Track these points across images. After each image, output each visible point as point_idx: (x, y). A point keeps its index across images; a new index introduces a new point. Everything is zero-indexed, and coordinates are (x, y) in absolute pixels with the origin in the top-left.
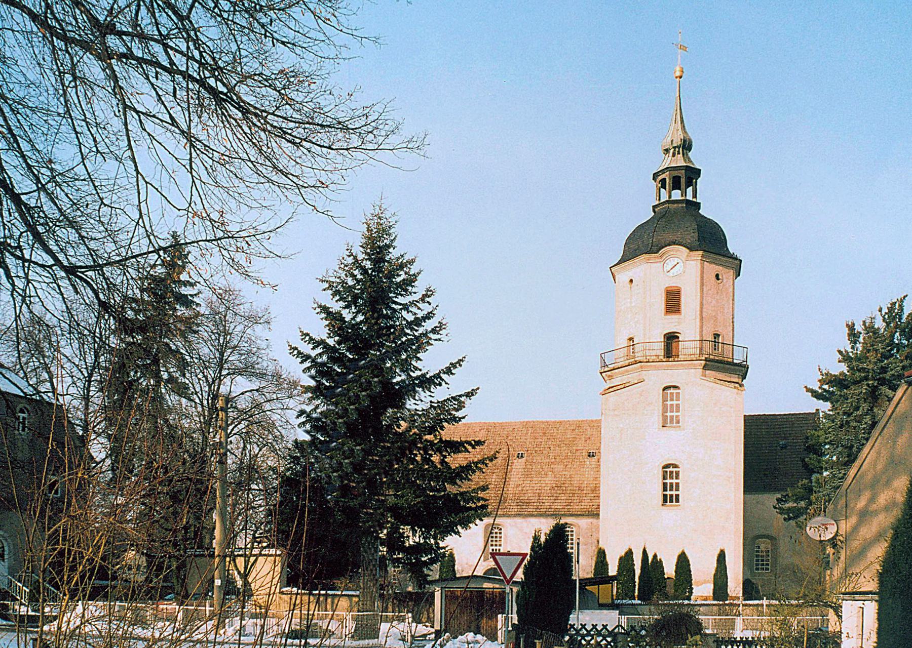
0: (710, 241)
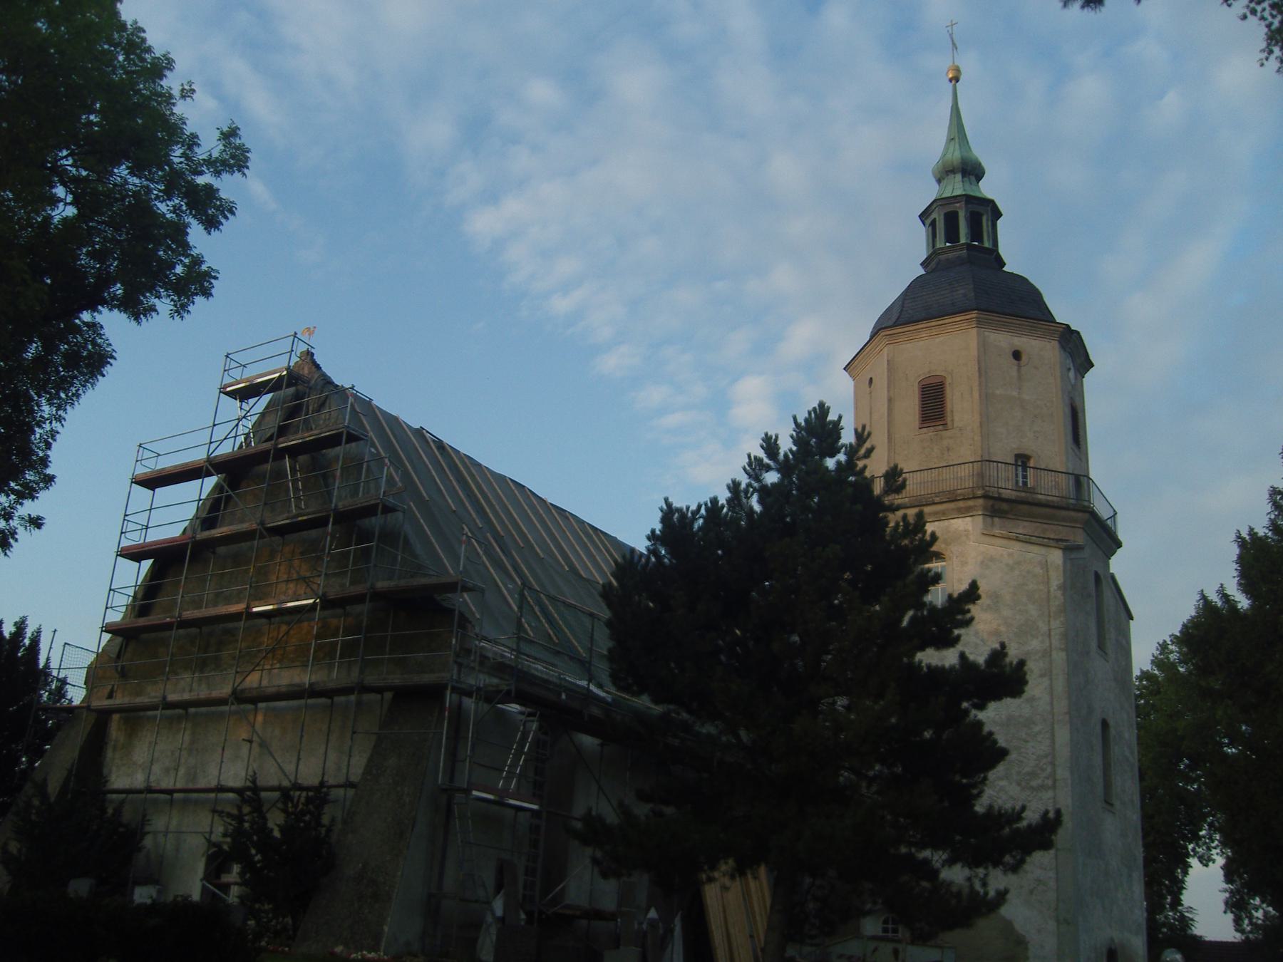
0: (1018, 304)
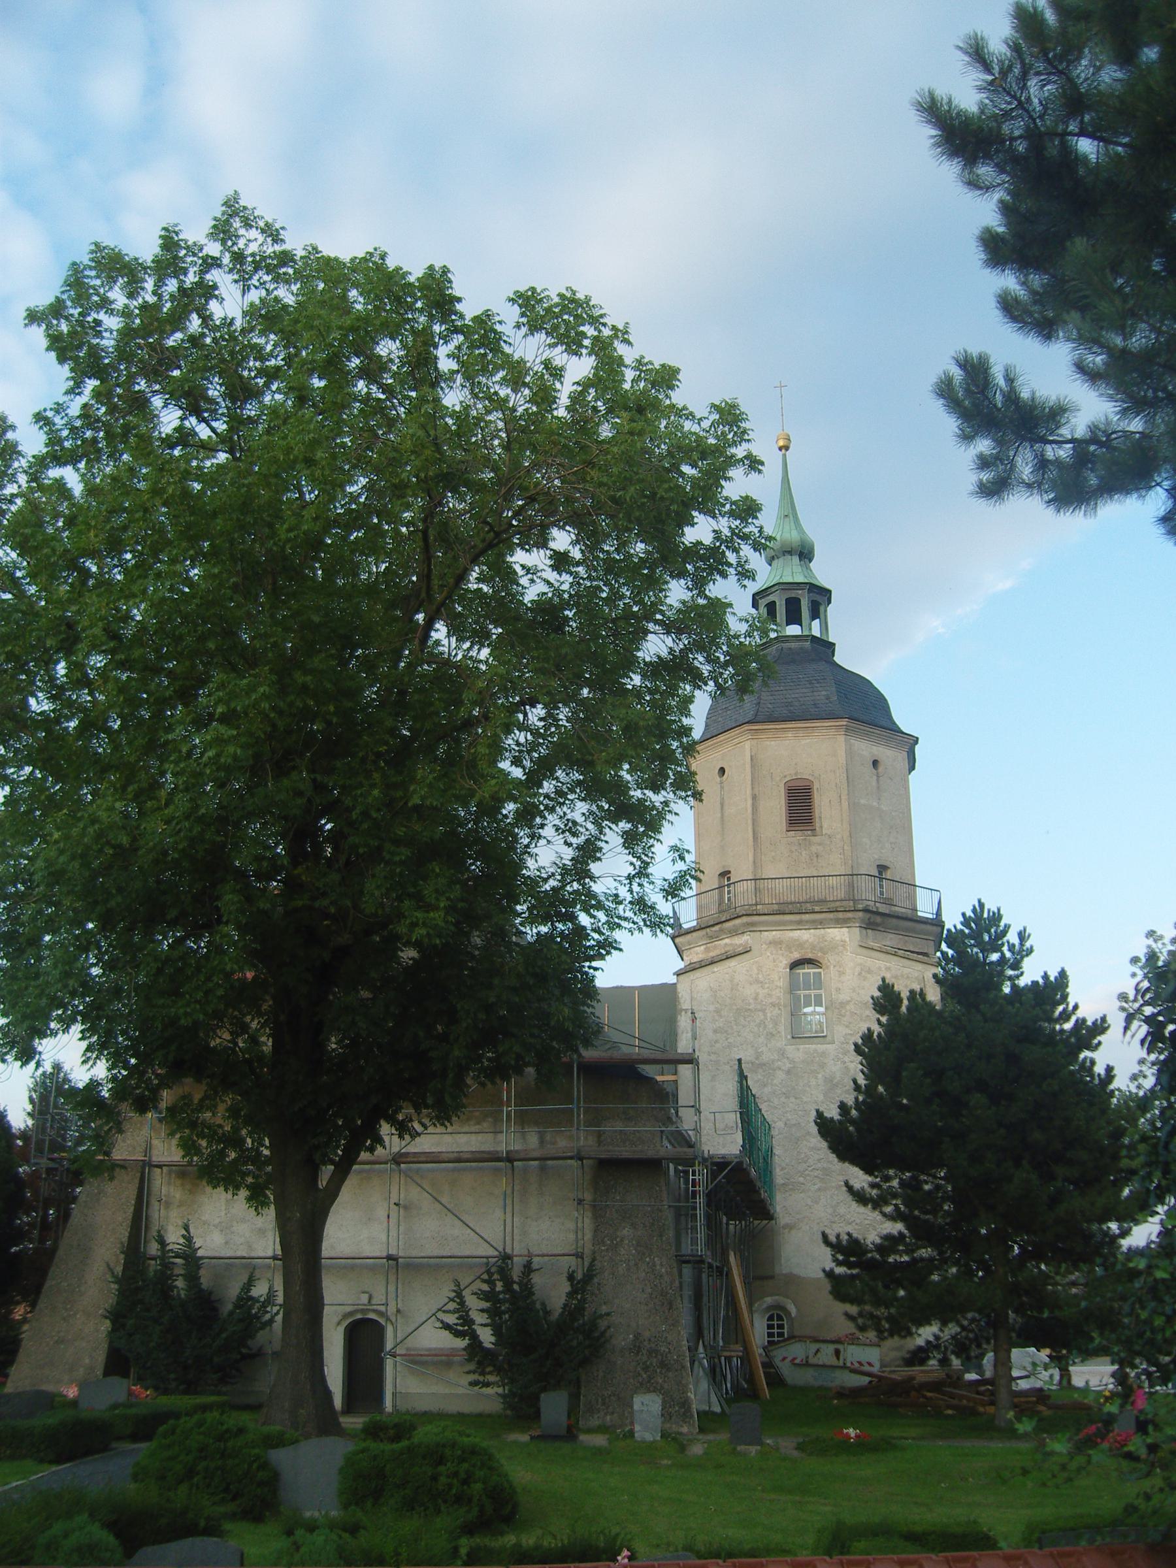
0: (863, 708)
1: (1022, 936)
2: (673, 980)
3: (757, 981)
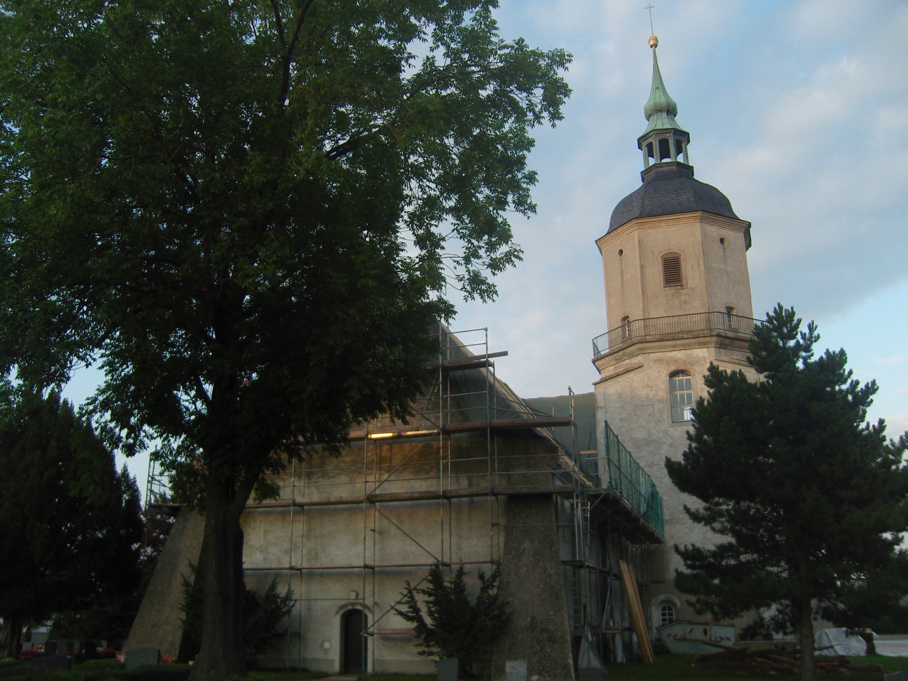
0: (713, 205)
1: (811, 328)
2: (591, 389)
3: (648, 386)
